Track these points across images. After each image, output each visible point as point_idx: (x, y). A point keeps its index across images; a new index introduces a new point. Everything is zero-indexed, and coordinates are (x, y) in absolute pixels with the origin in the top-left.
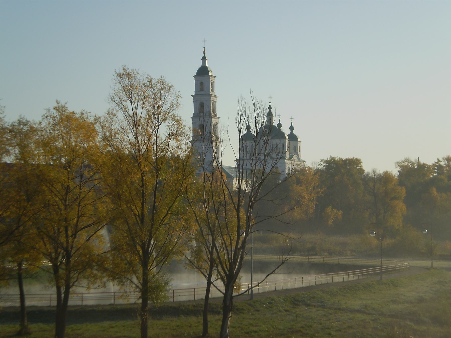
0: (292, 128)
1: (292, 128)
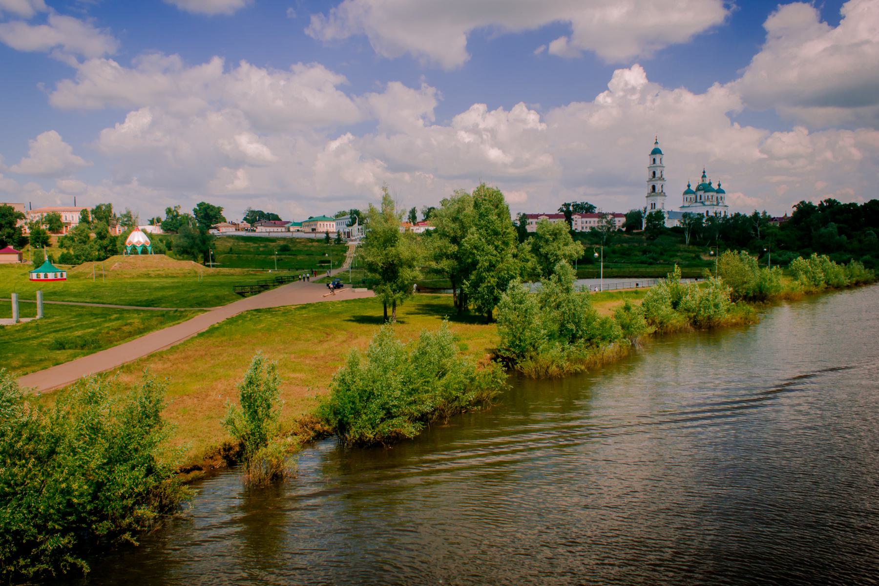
0: (719, 185)
1: (719, 185)
